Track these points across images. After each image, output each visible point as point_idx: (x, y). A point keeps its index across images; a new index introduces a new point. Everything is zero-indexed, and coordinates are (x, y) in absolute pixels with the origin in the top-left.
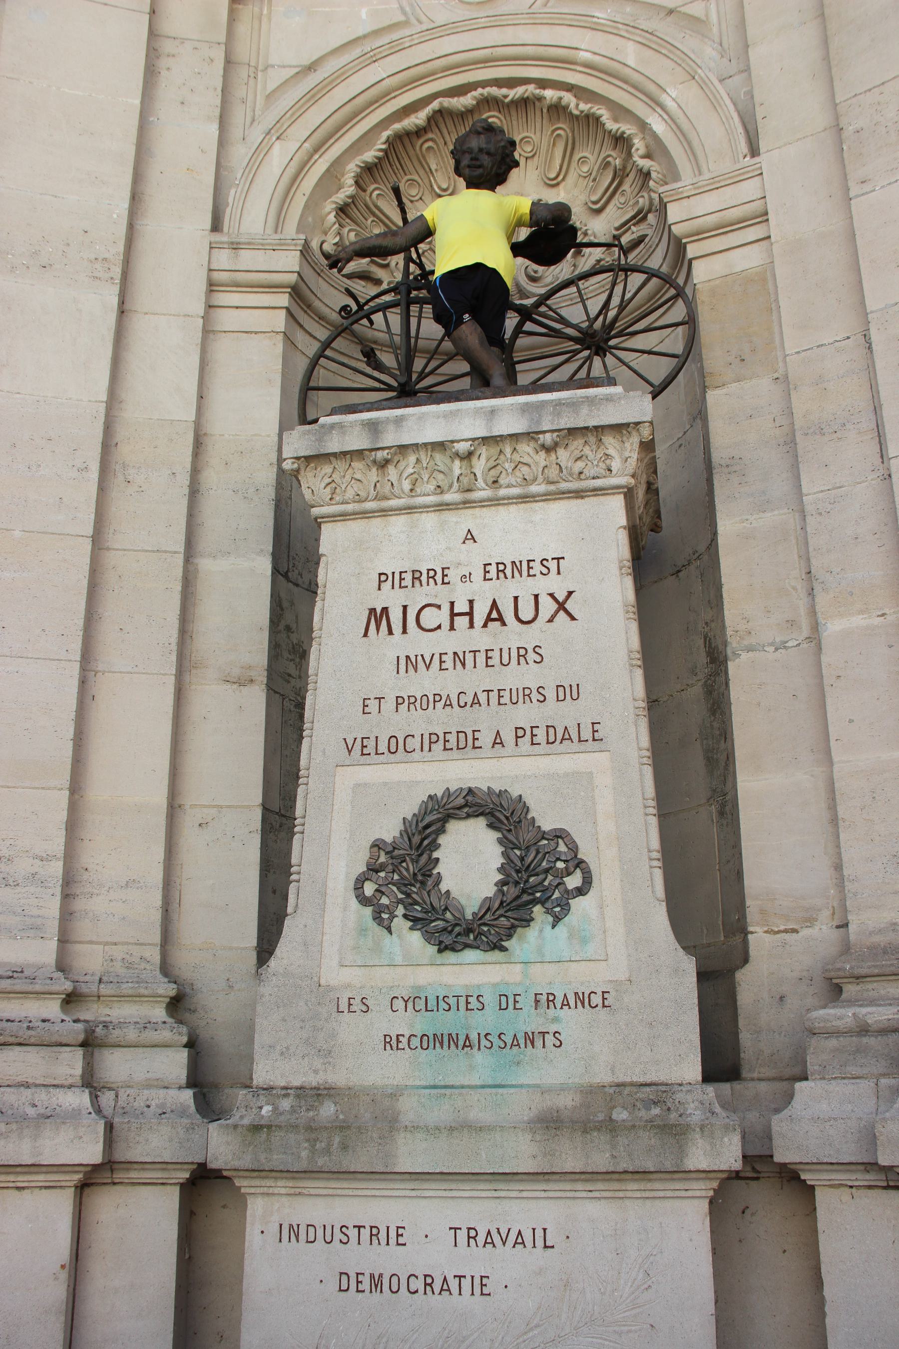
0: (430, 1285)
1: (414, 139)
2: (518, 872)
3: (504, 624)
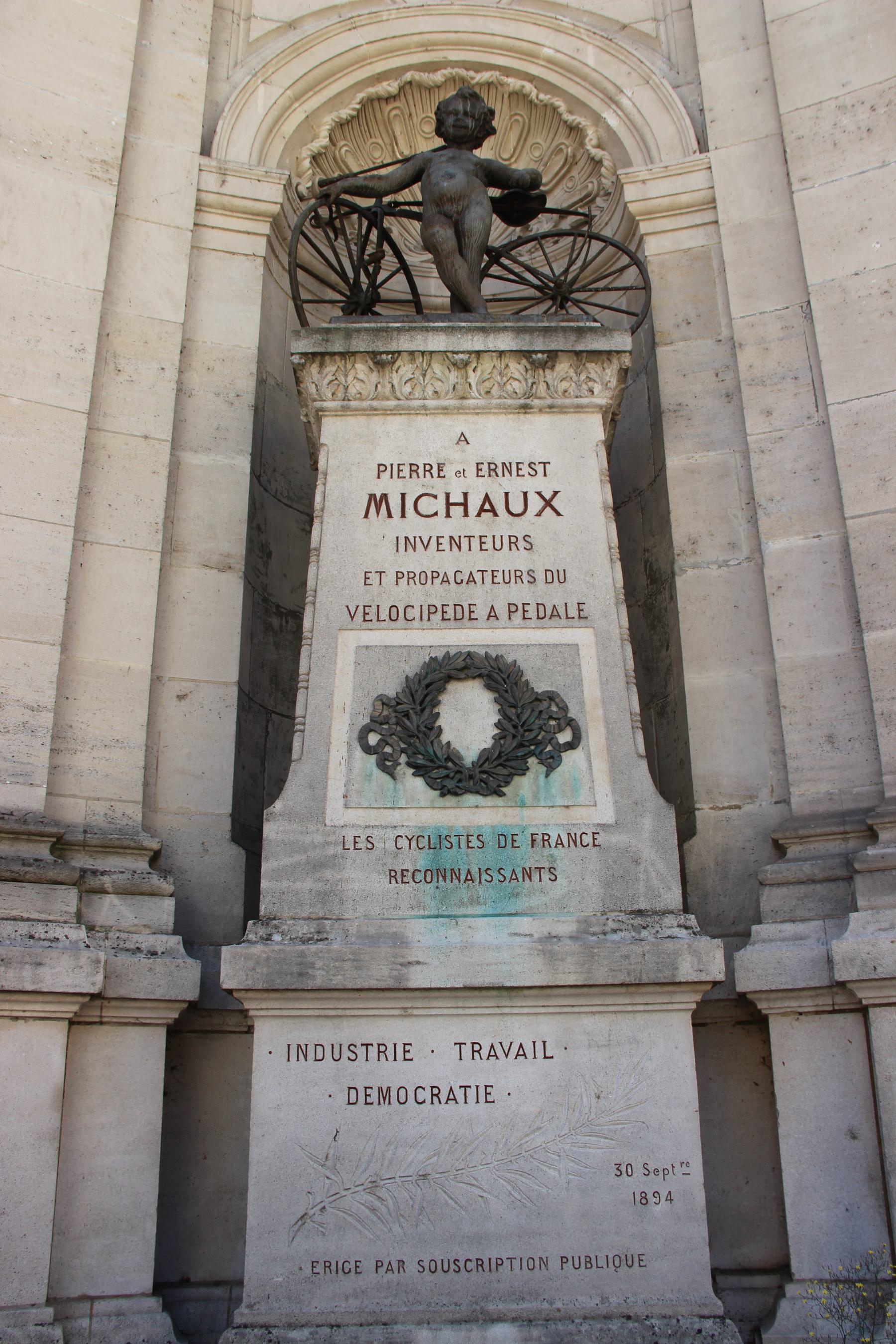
0: (437, 1095)
1: (383, 104)
2: (515, 727)
3: (496, 515)
